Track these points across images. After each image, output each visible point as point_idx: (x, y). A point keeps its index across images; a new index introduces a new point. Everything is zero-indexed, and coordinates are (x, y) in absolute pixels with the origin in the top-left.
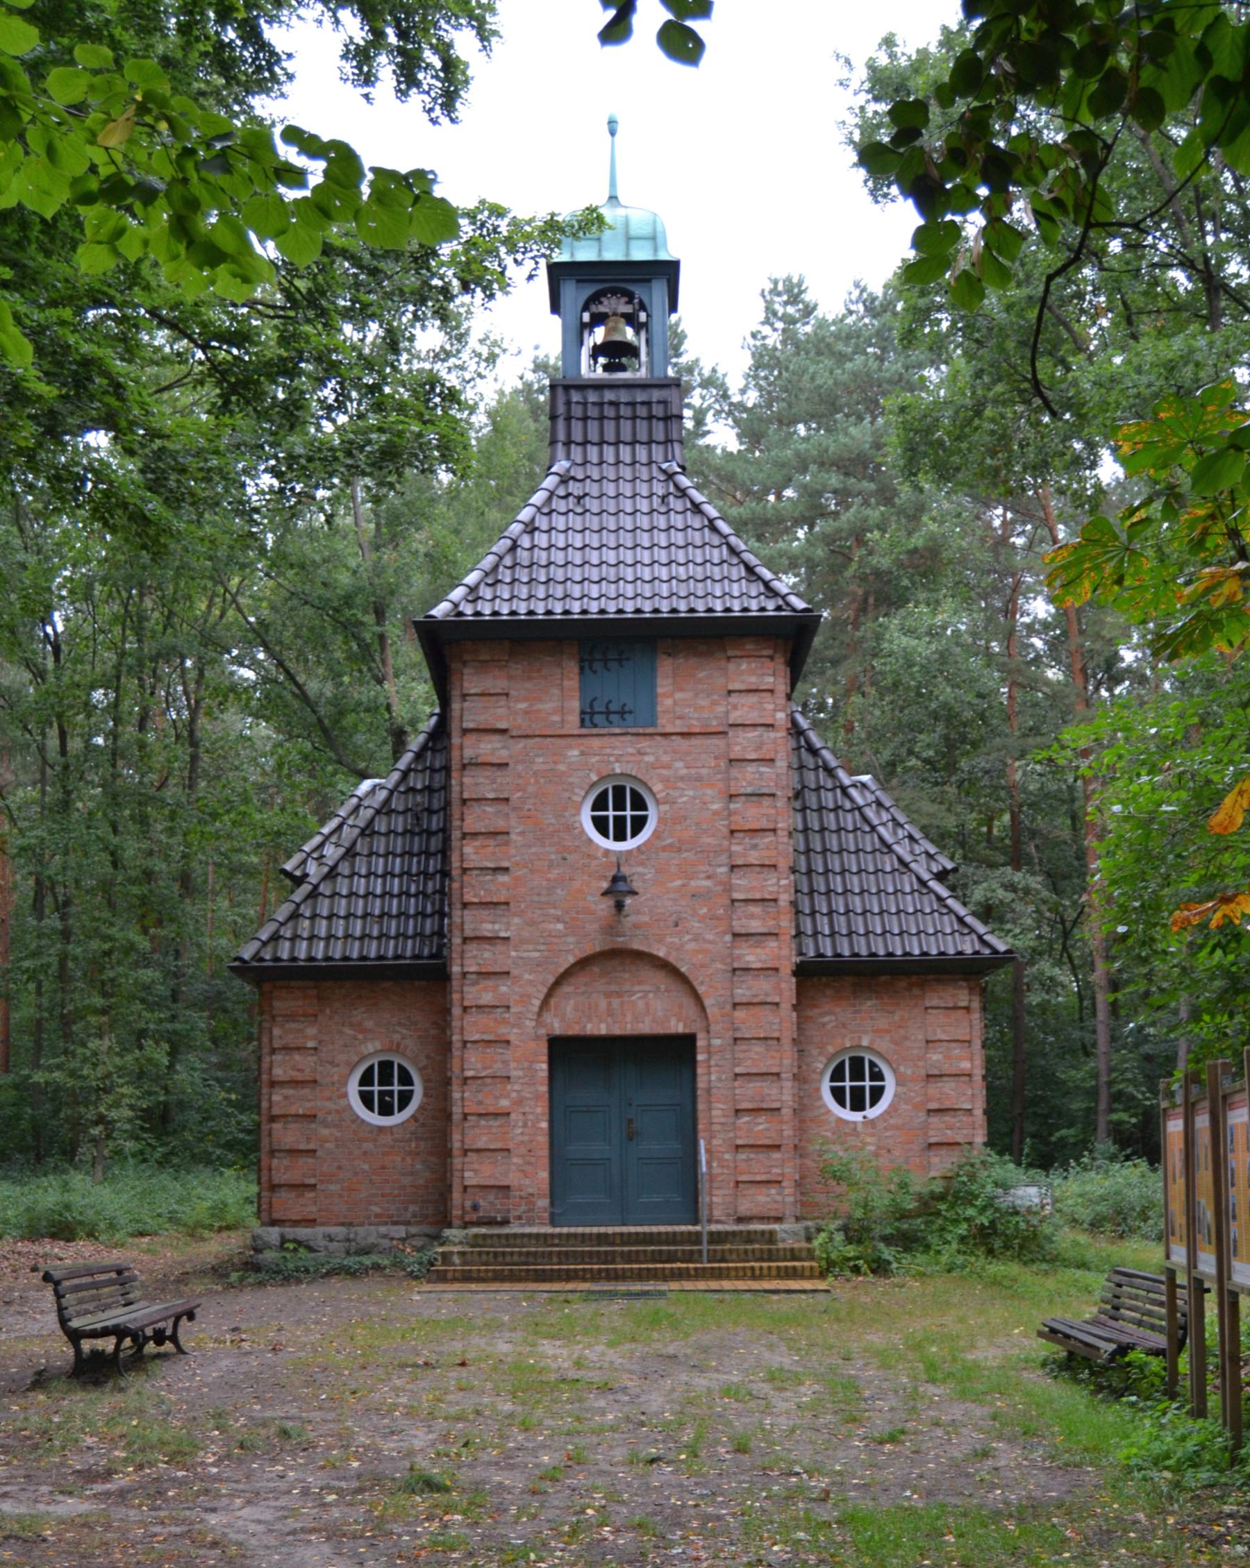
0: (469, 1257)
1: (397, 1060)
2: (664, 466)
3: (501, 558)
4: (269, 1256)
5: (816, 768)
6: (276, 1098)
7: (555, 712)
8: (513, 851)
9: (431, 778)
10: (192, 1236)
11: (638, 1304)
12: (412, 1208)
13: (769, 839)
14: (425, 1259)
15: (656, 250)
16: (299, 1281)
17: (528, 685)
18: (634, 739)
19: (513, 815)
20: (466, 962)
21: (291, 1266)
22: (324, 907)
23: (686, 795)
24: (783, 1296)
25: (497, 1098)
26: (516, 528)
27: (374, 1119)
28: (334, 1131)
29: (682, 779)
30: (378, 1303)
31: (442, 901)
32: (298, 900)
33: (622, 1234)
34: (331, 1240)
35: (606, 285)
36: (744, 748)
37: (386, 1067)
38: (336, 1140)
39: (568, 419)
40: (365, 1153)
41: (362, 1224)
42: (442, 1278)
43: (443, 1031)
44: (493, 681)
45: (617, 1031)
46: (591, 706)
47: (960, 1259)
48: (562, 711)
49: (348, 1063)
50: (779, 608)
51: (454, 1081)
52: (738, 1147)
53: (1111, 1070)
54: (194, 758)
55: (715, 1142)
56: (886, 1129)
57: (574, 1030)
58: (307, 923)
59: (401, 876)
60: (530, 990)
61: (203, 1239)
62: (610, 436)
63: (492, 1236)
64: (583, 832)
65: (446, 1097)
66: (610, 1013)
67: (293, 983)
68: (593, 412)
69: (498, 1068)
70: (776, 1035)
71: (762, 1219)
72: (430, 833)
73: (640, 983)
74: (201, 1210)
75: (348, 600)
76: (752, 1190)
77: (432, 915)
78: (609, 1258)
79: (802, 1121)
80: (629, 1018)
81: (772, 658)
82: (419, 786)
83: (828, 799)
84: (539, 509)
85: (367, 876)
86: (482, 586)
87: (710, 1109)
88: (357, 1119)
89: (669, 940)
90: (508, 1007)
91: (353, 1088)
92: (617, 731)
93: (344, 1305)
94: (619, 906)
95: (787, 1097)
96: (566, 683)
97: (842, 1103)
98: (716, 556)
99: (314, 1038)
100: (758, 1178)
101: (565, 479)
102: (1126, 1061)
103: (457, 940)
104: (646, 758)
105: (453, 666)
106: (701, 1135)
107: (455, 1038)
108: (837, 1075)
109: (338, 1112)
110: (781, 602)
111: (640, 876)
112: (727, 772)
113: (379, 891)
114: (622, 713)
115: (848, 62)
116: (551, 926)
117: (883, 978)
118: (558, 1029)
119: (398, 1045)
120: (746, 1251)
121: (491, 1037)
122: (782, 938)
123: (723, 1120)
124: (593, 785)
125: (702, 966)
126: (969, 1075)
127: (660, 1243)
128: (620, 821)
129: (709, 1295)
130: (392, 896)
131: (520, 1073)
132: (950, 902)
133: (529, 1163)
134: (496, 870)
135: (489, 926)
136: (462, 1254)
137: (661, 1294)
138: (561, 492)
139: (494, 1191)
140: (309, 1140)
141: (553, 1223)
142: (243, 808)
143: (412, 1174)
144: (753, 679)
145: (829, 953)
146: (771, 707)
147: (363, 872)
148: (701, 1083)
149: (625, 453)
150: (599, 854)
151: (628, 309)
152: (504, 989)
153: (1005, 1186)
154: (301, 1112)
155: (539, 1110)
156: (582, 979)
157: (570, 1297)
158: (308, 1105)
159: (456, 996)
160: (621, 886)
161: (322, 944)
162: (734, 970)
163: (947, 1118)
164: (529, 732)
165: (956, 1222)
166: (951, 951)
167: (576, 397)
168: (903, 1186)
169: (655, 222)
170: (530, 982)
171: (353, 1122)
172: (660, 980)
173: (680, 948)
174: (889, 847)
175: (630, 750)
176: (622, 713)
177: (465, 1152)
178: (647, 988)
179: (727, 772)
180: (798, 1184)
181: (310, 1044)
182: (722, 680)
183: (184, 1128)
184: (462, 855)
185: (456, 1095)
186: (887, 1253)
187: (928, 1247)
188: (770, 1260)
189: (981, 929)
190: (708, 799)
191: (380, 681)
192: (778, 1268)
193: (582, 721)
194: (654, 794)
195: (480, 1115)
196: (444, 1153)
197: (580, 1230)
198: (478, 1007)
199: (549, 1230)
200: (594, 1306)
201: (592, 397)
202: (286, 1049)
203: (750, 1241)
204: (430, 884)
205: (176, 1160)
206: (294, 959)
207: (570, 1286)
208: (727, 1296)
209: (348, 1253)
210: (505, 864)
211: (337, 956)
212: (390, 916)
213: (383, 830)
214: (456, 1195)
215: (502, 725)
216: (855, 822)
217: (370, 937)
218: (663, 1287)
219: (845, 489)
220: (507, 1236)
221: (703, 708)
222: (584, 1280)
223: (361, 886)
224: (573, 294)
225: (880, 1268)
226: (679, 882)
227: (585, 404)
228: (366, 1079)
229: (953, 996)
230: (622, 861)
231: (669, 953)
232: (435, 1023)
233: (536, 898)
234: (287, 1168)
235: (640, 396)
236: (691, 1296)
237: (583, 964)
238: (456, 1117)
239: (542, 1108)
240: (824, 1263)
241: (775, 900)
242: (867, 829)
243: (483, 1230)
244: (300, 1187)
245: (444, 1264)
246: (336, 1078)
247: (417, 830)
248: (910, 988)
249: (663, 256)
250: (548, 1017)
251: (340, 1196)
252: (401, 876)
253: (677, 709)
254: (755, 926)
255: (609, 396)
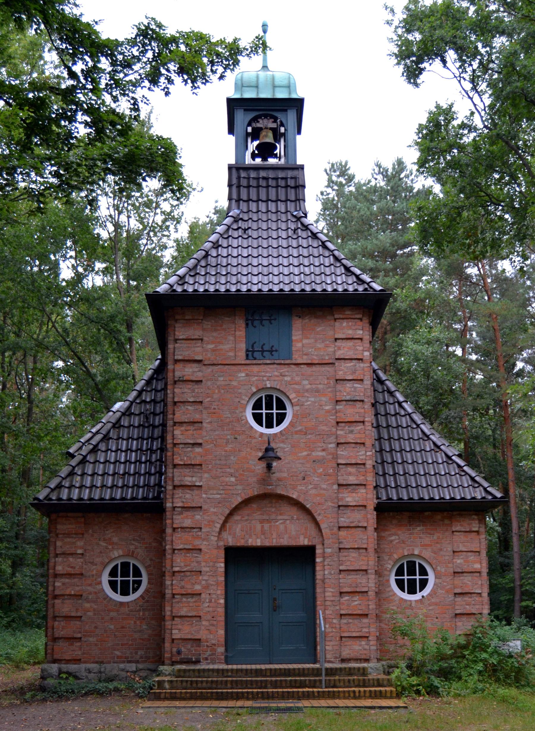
0: (175, 684)
1: (132, 561)
2: (295, 213)
3: (199, 261)
4: (51, 682)
5: (384, 391)
6: (57, 584)
7: (230, 350)
8: (204, 434)
9: (155, 396)
10: (17, 667)
11: (285, 717)
12: (140, 653)
13: (360, 427)
14: (147, 685)
15: (290, 93)
16: (68, 699)
17: (215, 334)
18: (278, 366)
19: (205, 412)
20: (175, 500)
21: (63, 688)
22: (89, 469)
23: (310, 400)
24: (377, 710)
25: (193, 584)
26: (208, 245)
27: (117, 597)
28: (93, 604)
29: (307, 391)
30: (116, 715)
31: (161, 466)
32: (74, 464)
33: (271, 670)
34: (90, 672)
35: (261, 113)
36: (345, 373)
37: (125, 566)
38: (94, 610)
39: (239, 187)
40: (112, 619)
41: (109, 662)
42: (158, 697)
43: (161, 544)
44: (194, 332)
45: (267, 544)
46: (253, 346)
47: (480, 686)
48: (235, 349)
49: (102, 563)
50: (366, 290)
51: (167, 574)
52: (341, 615)
53: (522, 578)
54: (30, 410)
55: (327, 612)
56: (429, 605)
57: (241, 543)
58: (79, 478)
59: (136, 451)
60: (214, 518)
61: (23, 669)
62: (263, 197)
63: (189, 670)
64: (247, 422)
65: (162, 584)
66: (263, 532)
67: (69, 514)
68: (253, 183)
69: (194, 566)
70: (365, 546)
71: (357, 660)
72: (154, 427)
73: (281, 514)
74: (22, 652)
75: (112, 318)
76: (350, 642)
77: (154, 474)
78: (263, 685)
79: (380, 600)
80: (274, 536)
81: (361, 319)
82: (148, 400)
83: (391, 409)
84: (221, 235)
85: (116, 451)
86: (187, 276)
87: (324, 592)
88: (107, 597)
89: (299, 488)
90: (201, 528)
91: (105, 578)
92: (268, 362)
93: (94, 716)
94: (269, 467)
95: (372, 584)
96: (238, 333)
97: (402, 589)
98: (327, 262)
99: (81, 548)
100: (354, 634)
101: (236, 220)
102: (529, 574)
103: (170, 488)
104: (286, 378)
105: (169, 322)
106: (318, 608)
107: (168, 547)
108: (400, 572)
109: (96, 593)
110: (366, 286)
111: (278, 446)
112: (335, 387)
113: (123, 460)
114: (271, 351)
115: (392, 11)
116: (227, 479)
117: (427, 514)
118: (231, 542)
119: (133, 552)
120: (349, 681)
121: (190, 547)
122: (368, 487)
123: (332, 599)
124: (254, 394)
125: (319, 504)
126: (479, 572)
127: (294, 675)
128: (269, 417)
129: (331, 710)
130: (131, 463)
131: (208, 569)
132: (465, 468)
133: (213, 625)
134: (194, 444)
135: (189, 479)
136: (171, 682)
137: (299, 709)
138: (235, 226)
139: (191, 642)
140: (77, 610)
141: (227, 663)
142: (54, 434)
143: (140, 631)
144: (350, 332)
145: (395, 498)
146: (361, 348)
147: (114, 449)
148: (319, 576)
149: (272, 207)
150: (257, 436)
151: (274, 125)
152: (198, 517)
153: (504, 640)
154: (73, 593)
155: (219, 592)
156: (245, 511)
157: (240, 711)
158: (77, 588)
159: (168, 522)
160: (271, 454)
161: (87, 491)
162: (339, 506)
163: (466, 598)
164: (215, 362)
165: (475, 662)
166: (469, 497)
167: (243, 174)
168: (444, 639)
169: (289, 78)
170: (215, 513)
171: (105, 599)
172: (294, 512)
173: (306, 493)
174: (428, 436)
175: (276, 373)
176: (271, 351)
177: (173, 618)
178: (285, 517)
179: (335, 387)
180: (378, 639)
181: (80, 551)
182: (331, 333)
183: (21, 608)
184: (173, 436)
185: (168, 583)
186: (436, 682)
187: (460, 678)
188: (364, 686)
189: (486, 484)
190: (324, 403)
191: (129, 362)
192: (370, 691)
193: (247, 355)
194: (290, 400)
195: (182, 595)
196: (161, 618)
197: (244, 667)
198: (182, 528)
199: (225, 667)
200: (256, 717)
201: (253, 174)
202: (64, 554)
203: (351, 674)
204: (154, 456)
205: (14, 625)
206: (70, 499)
207: (240, 703)
208: (342, 711)
209: (100, 681)
210: (200, 441)
211: (97, 497)
212: (129, 475)
213: (126, 424)
214: (167, 645)
215: (197, 358)
216: (407, 422)
217: (117, 487)
218: (300, 704)
219: (376, 268)
220: (199, 670)
221: (320, 349)
222: (248, 699)
223: (112, 457)
224: (242, 117)
225: (433, 691)
226: (305, 453)
227: (248, 178)
228: (113, 573)
229: (469, 524)
230: (271, 440)
231: (299, 496)
232: (155, 539)
233: (218, 462)
234: (63, 628)
235: (281, 174)
236: (319, 711)
237: (247, 502)
238: (168, 596)
239: (220, 591)
240: (399, 689)
241: (364, 464)
242: (415, 426)
243: (184, 667)
244: (71, 639)
245: (158, 688)
246: (94, 572)
247: (146, 425)
248: (442, 519)
249: (294, 96)
250: (225, 535)
251: (96, 645)
252: (136, 451)
253: (304, 349)
254: (352, 480)
255: (263, 174)
